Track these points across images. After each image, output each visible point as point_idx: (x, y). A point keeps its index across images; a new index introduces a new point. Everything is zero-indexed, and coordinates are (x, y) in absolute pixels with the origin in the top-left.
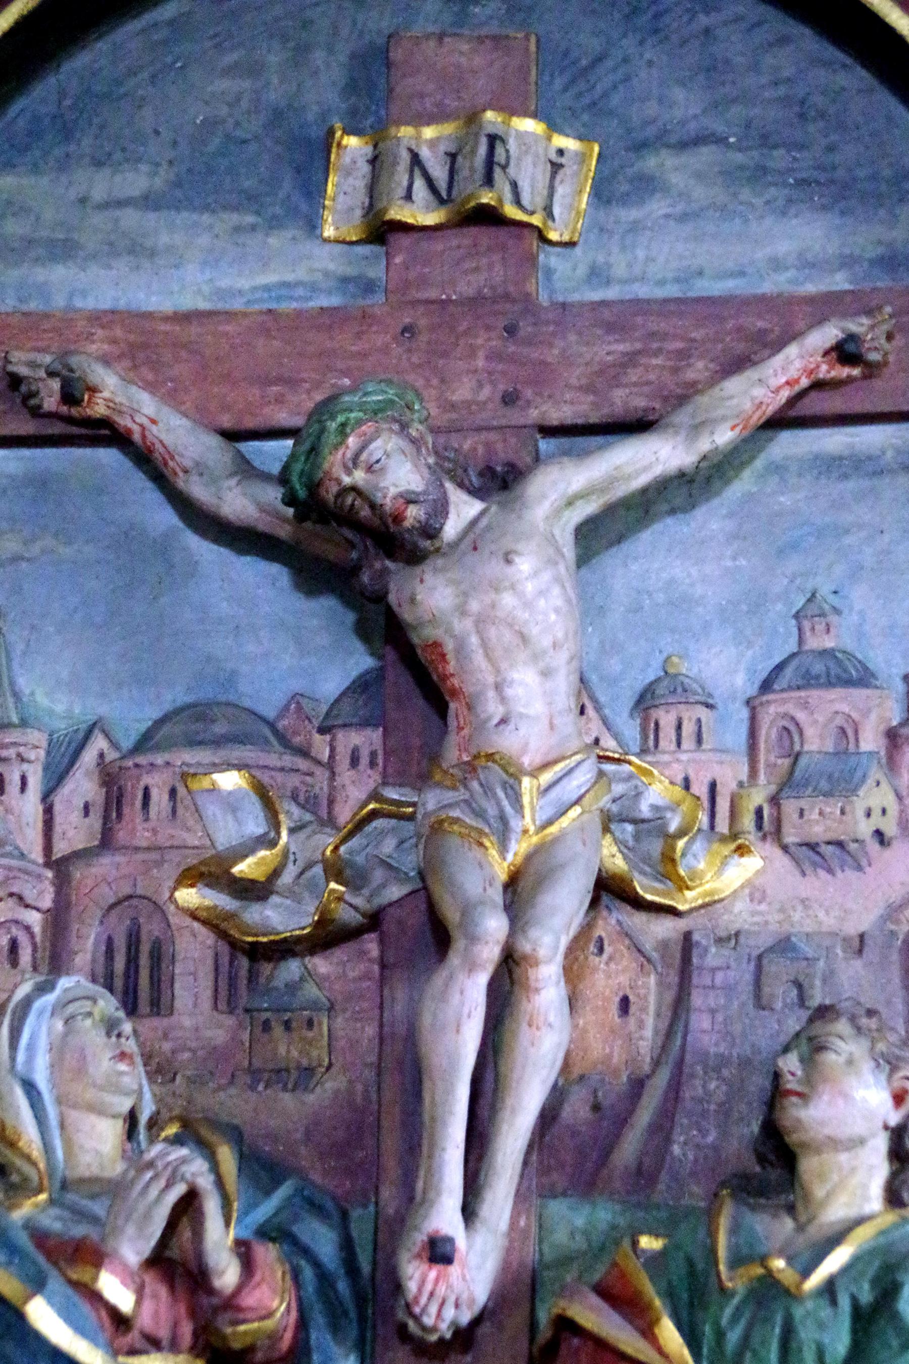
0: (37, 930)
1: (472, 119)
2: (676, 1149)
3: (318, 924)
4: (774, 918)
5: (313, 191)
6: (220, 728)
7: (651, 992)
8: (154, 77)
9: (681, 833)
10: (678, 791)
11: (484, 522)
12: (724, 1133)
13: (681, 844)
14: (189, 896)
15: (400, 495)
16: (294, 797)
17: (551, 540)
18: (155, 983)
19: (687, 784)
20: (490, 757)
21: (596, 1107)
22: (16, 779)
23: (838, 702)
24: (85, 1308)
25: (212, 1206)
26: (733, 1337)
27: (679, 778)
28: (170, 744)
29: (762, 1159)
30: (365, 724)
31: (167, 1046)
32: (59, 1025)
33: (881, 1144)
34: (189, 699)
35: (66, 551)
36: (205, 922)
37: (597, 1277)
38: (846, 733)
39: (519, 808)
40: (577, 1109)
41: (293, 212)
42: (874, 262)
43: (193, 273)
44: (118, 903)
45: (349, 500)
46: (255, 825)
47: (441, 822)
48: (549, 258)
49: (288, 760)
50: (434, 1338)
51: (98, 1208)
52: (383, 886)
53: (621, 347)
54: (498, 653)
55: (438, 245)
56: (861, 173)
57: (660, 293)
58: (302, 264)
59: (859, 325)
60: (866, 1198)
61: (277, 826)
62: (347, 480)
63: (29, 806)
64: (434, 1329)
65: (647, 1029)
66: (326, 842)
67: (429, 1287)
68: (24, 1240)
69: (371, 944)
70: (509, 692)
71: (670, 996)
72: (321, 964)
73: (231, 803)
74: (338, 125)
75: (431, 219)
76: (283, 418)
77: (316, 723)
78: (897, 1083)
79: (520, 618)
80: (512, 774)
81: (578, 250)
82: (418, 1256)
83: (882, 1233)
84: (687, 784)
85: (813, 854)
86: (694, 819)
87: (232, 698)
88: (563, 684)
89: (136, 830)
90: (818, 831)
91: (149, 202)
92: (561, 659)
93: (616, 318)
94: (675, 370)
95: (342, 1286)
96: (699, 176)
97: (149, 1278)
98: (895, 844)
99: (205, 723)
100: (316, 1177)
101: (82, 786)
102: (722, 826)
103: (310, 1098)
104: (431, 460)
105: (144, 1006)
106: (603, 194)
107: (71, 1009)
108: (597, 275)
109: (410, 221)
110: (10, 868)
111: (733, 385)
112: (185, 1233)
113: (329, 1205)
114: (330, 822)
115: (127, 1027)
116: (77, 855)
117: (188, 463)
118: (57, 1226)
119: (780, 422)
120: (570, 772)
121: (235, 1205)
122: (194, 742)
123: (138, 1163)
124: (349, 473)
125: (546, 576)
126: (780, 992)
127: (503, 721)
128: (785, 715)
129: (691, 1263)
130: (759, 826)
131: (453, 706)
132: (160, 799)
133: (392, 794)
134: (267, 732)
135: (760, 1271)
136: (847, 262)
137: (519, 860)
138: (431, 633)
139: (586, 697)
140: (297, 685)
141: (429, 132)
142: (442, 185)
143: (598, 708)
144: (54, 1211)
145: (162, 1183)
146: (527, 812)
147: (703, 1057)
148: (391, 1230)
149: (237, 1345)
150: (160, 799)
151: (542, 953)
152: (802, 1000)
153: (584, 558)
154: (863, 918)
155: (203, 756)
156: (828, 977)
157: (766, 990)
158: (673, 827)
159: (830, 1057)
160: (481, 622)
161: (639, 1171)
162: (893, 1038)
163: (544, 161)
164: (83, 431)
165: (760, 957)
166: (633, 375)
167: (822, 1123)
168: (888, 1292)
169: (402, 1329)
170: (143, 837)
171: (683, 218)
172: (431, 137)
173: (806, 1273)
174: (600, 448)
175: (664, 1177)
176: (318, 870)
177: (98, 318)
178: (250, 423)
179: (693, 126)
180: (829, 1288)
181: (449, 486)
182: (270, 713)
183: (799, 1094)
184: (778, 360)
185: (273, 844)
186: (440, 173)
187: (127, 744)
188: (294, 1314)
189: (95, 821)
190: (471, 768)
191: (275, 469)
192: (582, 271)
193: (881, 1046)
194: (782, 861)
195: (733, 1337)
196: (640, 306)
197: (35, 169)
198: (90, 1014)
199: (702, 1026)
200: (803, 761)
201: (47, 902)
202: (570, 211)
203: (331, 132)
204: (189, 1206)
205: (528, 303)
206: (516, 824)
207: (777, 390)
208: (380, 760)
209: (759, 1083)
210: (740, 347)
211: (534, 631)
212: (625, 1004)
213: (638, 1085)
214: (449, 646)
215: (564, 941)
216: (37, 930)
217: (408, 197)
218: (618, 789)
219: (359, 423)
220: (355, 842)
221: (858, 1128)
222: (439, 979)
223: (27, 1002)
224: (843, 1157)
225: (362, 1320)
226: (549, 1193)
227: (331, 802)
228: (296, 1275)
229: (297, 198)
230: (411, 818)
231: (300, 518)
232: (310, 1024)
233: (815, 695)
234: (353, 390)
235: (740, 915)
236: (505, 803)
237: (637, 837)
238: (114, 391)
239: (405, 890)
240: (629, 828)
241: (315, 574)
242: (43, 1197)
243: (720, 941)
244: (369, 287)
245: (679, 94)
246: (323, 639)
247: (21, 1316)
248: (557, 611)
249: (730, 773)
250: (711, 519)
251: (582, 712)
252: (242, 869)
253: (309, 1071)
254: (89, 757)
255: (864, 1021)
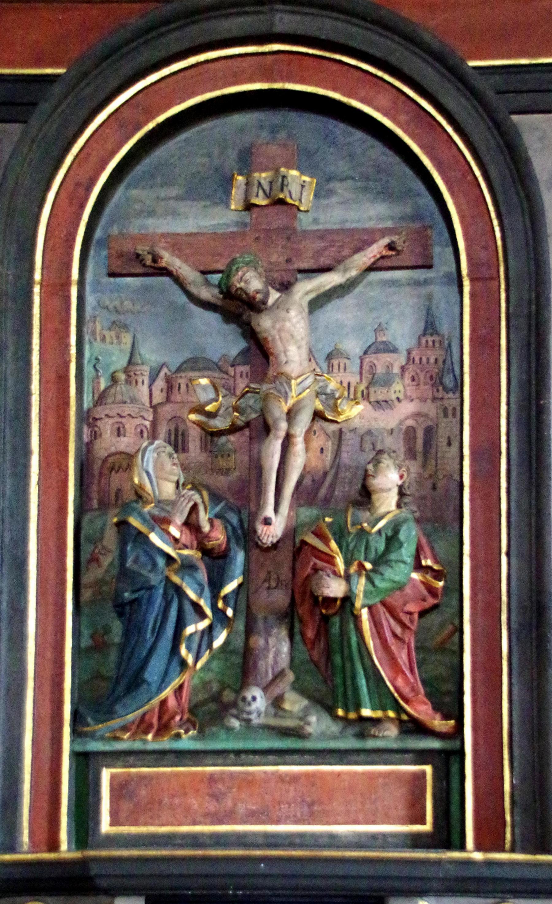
0: (148, 426)
1: (277, 171)
2: (336, 493)
3: (231, 426)
4: (367, 424)
5: (228, 194)
6: (201, 365)
7: (330, 446)
8: (205, 207)
9: (339, 398)
10: (339, 385)
11: (280, 300)
12: (350, 487)
13: (339, 401)
14: (193, 417)
15: (255, 291)
16: (223, 387)
17: (301, 305)
18: (183, 441)
19: (341, 383)
20: (282, 374)
21: (313, 481)
22: (141, 381)
23: (386, 358)
24: (167, 537)
25: (201, 508)
26: (352, 545)
27: (339, 381)
28: (185, 370)
29: (361, 495)
30: (245, 364)
31: (187, 462)
32: (156, 455)
33: (395, 490)
34: (191, 356)
35: (154, 310)
36: (197, 425)
37: (313, 529)
38: (389, 367)
39: (291, 390)
40: (307, 481)
41: (222, 201)
42: (400, 218)
43: (191, 221)
44: (172, 418)
45: (239, 292)
46: (212, 395)
47: (267, 394)
48: (301, 216)
49: (222, 375)
50: (266, 546)
51: (168, 508)
52: (251, 414)
53: (323, 244)
54: (285, 341)
55: (266, 211)
56: (396, 190)
57: (334, 227)
58: (223, 218)
59: (395, 238)
60: (391, 506)
61: (218, 395)
62: (238, 286)
63: (145, 389)
64: (265, 544)
65: (329, 456)
66: (233, 401)
67: (264, 532)
68: (148, 517)
69: (247, 432)
70: (288, 353)
71: (336, 447)
72: (232, 438)
73: (204, 388)
74: (236, 173)
75: (264, 202)
76: (220, 267)
77: (230, 363)
78: (401, 472)
79: (291, 330)
80: (289, 379)
81: (309, 214)
82: (261, 523)
83: (395, 516)
84: (341, 383)
85: (378, 405)
86: (343, 394)
87: (204, 356)
88: (304, 352)
89: (177, 397)
90: (380, 398)
91: (178, 198)
92: (304, 343)
93: (322, 235)
94: (339, 252)
95: (239, 532)
96: (346, 189)
97: (184, 528)
98: (403, 402)
99: (196, 364)
100: (232, 500)
101: (160, 383)
102: (352, 396)
103: (230, 478)
104: (264, 280)
105: (180, 450)
106: (317, 196)
107: (158, 450)
108: (316, 221)
109: (258, 203)
110: (140, 408)
111: (357, 257)
112: (194, 516)
113: (235, 509)
114: (234, 394)
115: (175, 456)
116: (159, 404)
117: (190, 281)
118: (157, 513)
119: (371, 268)
120: (306, 379)
121: (208, 508)
122: (193, 369)
123: (179, 495)
124: (239, 283)
125: (300, 317)
126: (368, 446)
127: (286, 362)
128: (371, 362)
129: (340, 526)
130: (363, 396)
131: (271, 358)
132: (183, 387)
133: (253, 386)
134: (215, 366)
135: (360, 527)
136: (392, 218)
137: (291, 406)
138: (265, 335)
139: (311, 355)
140: (224, 352)
141: (264, 175)
142: (268, 191)
143: (315, 359)
144: (157, 509)
145: (187, 501)
146: (293, 391)
147: (345, 465)
148: (253, 516)
149: (209, 547)
150: (183, 387)
151: (298, 433)
152: (374, 449)
153: (311, 312)
154: (393, 423)
155: (197, 374)
156: (382, 441)
157: (364, 446)
158: (337, 396)
159: (382, 465)
160: (279, 331)
161: (325, 498)
162: (401, 459)
163: (299, 183)
164: (158, 271)
165: (363, 435)
166: (327, 253)
167: (379, 484)
168: (396, 532)
169: (257, 543)
170: (178, 398)
171: (342, 203)
172: (264, 176)
173: (373, 527)
174: (316, 276)
175: (333, 500)
176: (231, 409)
177: (163, 235)
178: (209, 268)
179: (345, 174)
180: (379, 532)
181: (270, 288)
182: (215, 359)
183: (373, 476)
184: (371, 249)
185: (217, 401)
186: (267, 188)
187: (174, 369)
188: (226, 539)
189: (164, 394)
190: (276, 377)
191: (217, 283)
192: (311, 220)
193: (397, 462)
194: (369, 407)
195: (352, 545)
196: (327, 231)
197: (143, 188)
198: (164, 452)
199: (345, 458)
200: (376, 376)
201: (151, 418)
202: (307, 200)
203: (233, 175)
204: (194, 508)
205: (295, 231)
206: (290, 394)
207: (370, 259)
208: (249, 374)
209: (361, 473)
210: (358, 245)
211: (295, 334)
212: (322, 450)
213: (325, 474)
214: (270, 339)
215: (304, 431)
216: (148, 426)
217: (257, 196)
218: (321, 384)
219: (243, 267)
220: (242, 400)
221: (390, 486)
222: (267, 441)
223: (146, 448)
224: (385, 494)
225: (245, 542)
226: (300, 506)
227: (234, 389)
228: (226, 528)
229: (224, 197)
230: (258, 393)
231: (225, 298)
232: (229, 455)
233: (380, 355)
234: (240, 257)
235: (357, 423)
236: (287, 388)
237: (326, 399)
238: (168, 259)
239: (258, 415)
240: (324, 396)
241: (229, 316)
242: (153, 505)
243: (351, 431)
244: (245, 225)
245: (341, 163)
246: (231, 337)
247: (147, 538)
248: (302, 328)
249: (354, 379)
250: (349, 300)
251: (310, 360)
252: (208, 408)
253: (229, 469)
254: (162, 374)
255: (392, 454)
